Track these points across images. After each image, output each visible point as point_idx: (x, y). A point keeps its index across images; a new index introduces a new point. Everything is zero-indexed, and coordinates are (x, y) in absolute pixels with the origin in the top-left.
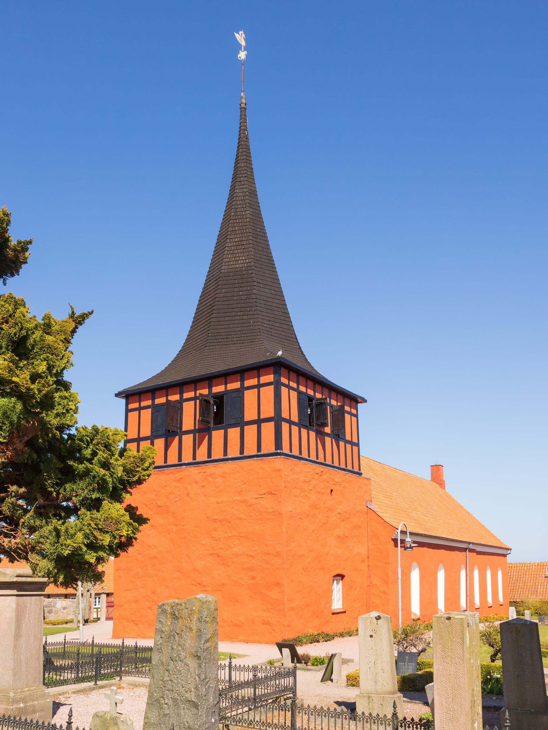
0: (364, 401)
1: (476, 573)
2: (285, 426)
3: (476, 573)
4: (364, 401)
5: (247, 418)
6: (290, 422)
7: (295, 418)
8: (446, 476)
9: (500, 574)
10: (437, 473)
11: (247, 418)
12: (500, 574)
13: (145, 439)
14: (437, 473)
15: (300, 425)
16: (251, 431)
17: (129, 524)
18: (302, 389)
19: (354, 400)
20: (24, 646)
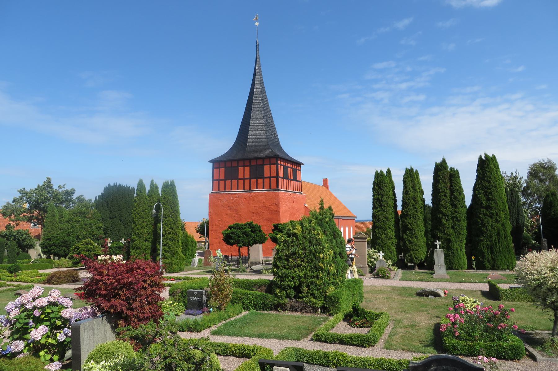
0: (303, 164)
1: (347, 229)
2: (280, 179)
3: (347, 229)
4: (303, 164)
5: (265, 176)
6: (281, 178)
7: (282, 176)
8: (329, 183)
9: (352, 229)
10: (325, 181)
11: (265, 176)
12: (352, 229)
13: (222, 180)
14: (325, 181)
15: (284, 178)
16: (267, 181)
17: (449, 235)
18: (284, 164)
19: (299, 164)
20: (168, 261)
